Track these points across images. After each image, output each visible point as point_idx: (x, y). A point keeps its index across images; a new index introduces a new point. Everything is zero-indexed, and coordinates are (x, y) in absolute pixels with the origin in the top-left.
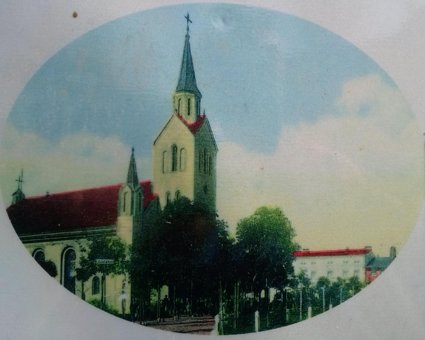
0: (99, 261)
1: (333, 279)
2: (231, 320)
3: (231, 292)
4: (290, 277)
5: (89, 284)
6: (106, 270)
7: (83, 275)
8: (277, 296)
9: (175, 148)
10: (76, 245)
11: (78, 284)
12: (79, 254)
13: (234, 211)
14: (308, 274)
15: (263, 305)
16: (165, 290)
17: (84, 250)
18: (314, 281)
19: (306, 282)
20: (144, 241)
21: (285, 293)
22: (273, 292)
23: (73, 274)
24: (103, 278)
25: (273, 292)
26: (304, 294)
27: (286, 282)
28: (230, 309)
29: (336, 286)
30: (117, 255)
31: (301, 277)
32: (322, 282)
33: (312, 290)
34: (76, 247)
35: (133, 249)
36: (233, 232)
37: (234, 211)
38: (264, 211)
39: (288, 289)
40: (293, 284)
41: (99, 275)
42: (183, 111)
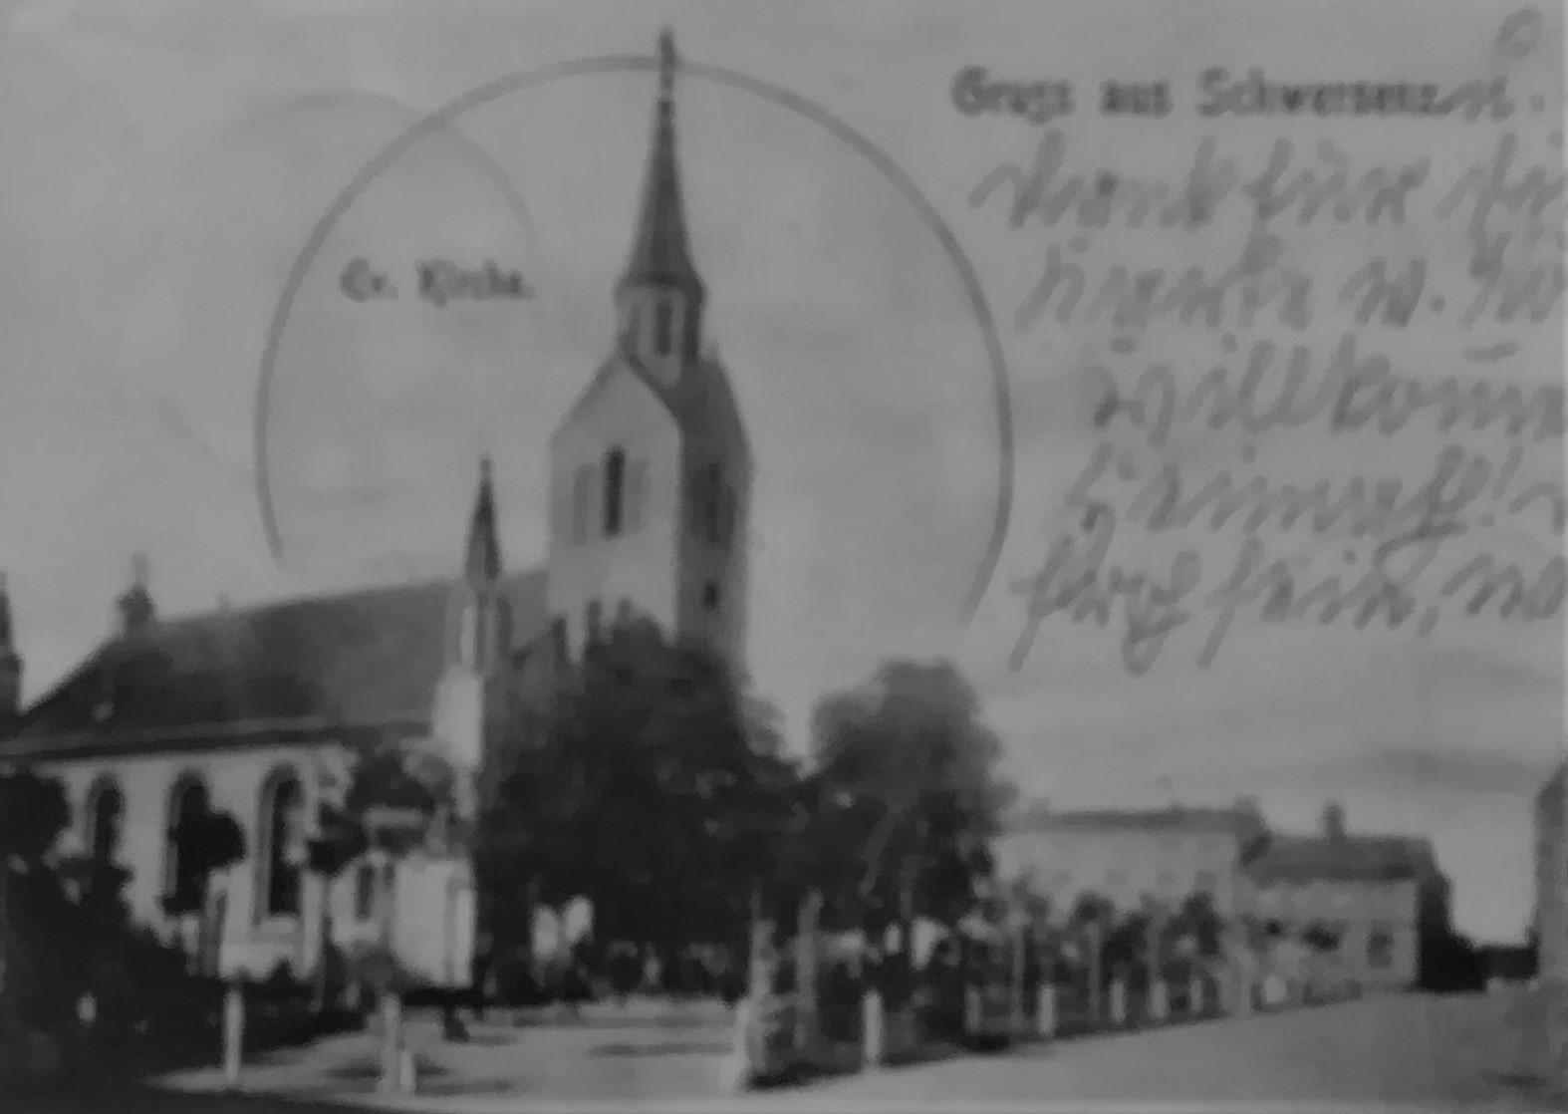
0: (378, 817)
1: (1125, 902)
2: (779, 1042)
3: (786, 932)
4: (981, 889)
5: (345, 886)
6: (396, 842)
7: (327, 858)
8: (941, 948)
9: (615, 464)
10: (306, 763)
11: (311, 887)
12: (313, 793)
13: (795, 678)
14: (1041, 886)
15: (892, 977)
16: (579, 916)
17: (327, 781)
18: (1063, 905)
19: (1038, 907)
20: (519, 776)
21: (965, 942)
22: (926, 935)
23: (296, 854)
24: (390, 873)
25: (926, 935)
26: (1031, 948)
27: (969, 903)
28: (784, 982)
29: (1136, 926)
30: (426, 797)
31: (1021, 888)
32: (1090, 909)
33: (1057, 937)
34: (308, 776)
35: (480, 780)
36: (798, 742)
37: (795, 678)
38: (900, 674)
39: (975, 926)
40: (992, 911)
41: (377, 858)
42: (646, 343)
